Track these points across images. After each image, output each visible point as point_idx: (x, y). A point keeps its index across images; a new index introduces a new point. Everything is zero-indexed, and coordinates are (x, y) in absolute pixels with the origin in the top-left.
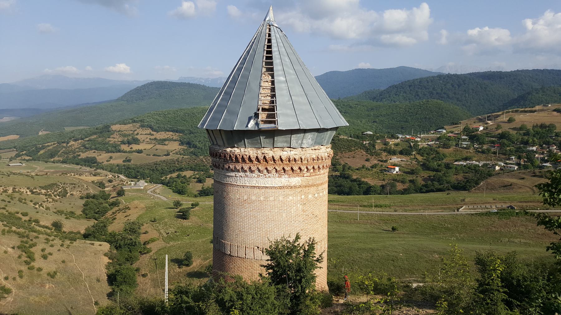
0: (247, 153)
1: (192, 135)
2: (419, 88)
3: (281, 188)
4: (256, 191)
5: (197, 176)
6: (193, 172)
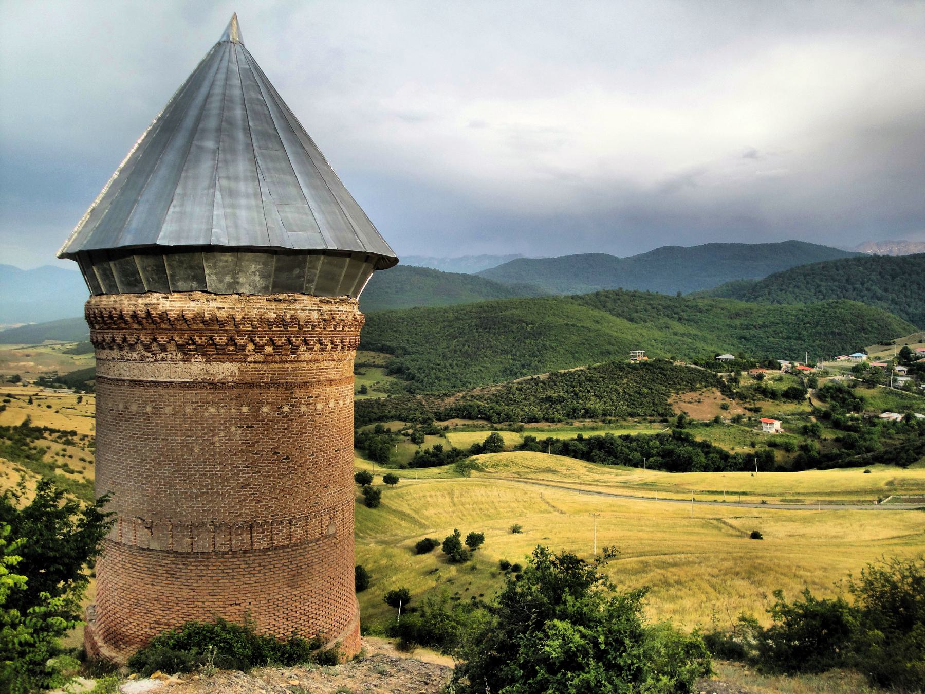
0: (117, 306)
1: (408, 357)
2: (821, 280)
3: (185, 386)
4: (138, 391)
5: (410, 431)
6: (404, 423)
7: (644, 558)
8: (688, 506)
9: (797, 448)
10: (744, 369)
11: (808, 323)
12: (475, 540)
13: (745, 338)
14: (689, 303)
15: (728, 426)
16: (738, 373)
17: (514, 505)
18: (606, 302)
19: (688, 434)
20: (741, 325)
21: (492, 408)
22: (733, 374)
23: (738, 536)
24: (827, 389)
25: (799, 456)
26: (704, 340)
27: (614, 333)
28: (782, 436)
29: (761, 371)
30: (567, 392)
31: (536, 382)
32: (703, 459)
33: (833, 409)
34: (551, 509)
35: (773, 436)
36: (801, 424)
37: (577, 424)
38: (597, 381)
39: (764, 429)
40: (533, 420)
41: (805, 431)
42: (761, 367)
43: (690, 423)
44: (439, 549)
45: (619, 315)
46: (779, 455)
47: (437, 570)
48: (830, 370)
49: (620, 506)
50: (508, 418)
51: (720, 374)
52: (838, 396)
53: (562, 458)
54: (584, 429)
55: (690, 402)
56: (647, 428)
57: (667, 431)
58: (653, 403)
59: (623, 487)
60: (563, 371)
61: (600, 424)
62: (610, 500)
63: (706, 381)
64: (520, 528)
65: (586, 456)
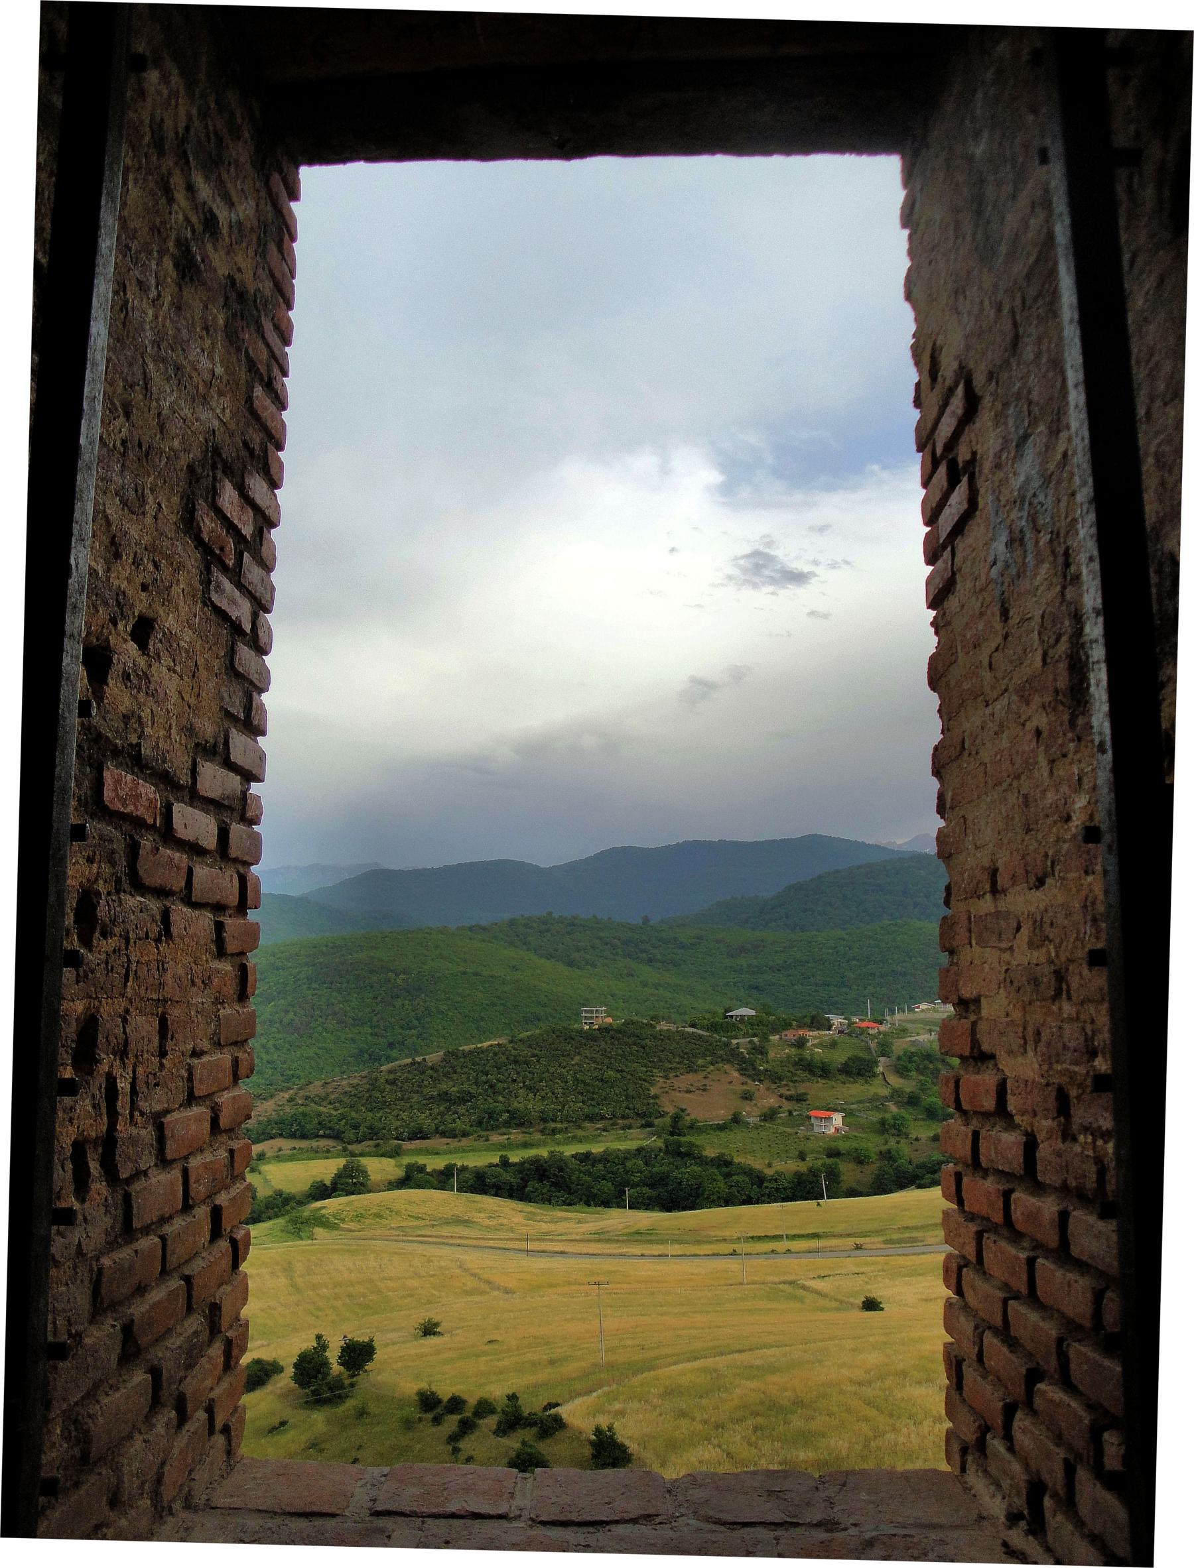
7: (709, 1362)
8: (732, 1264)
9: (874, 1157)
10: (774, 1031)
11: (854, 959)
12: (358, 1355)
15: (757, 1127)
16: (765, 1039)
17: (414, 1283)
19: (691, 1144)
20: (749, 966)
21: (343, 1116)
22: (756, 1039)
23: (837, 1309)
24: (910, 1057)
25: (881, 1168)
28: (846, 1138)
29: (801, 1033)
30: (476, 1083)
31: (421, 1067)
33: (923, 1088)
34: (483, 1286)
35: (832, 1138)
36: (875, 1117)
37: (496, 1138)
39: (816, 1129)
40: (418, 1134)
41: (883, 1127)
42: (799, 1027)
43: (691, 1127)
44: (285, 1380)
45: (549, 957)
46: (848, 1172)
47: (283, 1424)
48: (908, 1026)
49: (610, 1272)
50: (373, 1133)
51: (734, 1041)
52: (926, 1068)
53: (478, 1197)
54: (509, 1146)
56: (619, 1139)
57: (654, 1142)
58: (627, 1097)
59: (599, 1241)
60: (466, 1048)
61: (538, 1136)
62: (585, 1263)
64: (437, 1325)
65: (516, 1192)
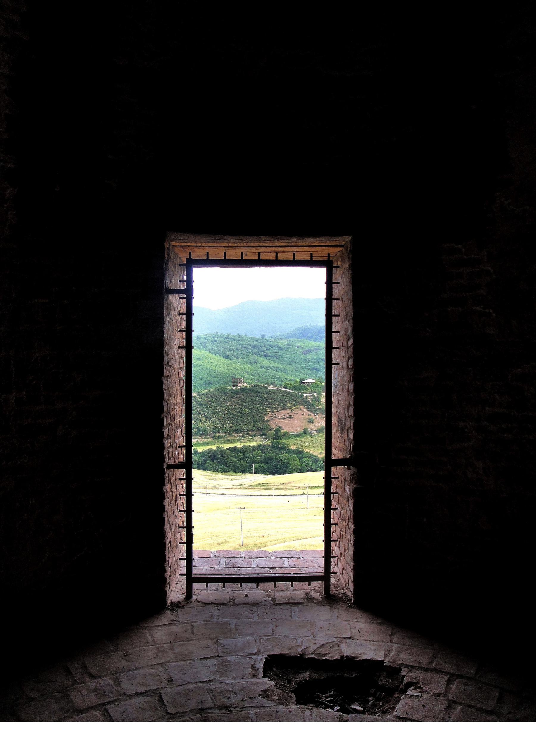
13: (316, 369)
14: (271, 343)
18: (205, 343)
19: (284, 443)
22: (315, 394)
26: (285, 371)
27: (214, 368)
32: (298, 463)
38: (206, 405)
51: (305, 395)
55: (283, 419)
56: (250, 441)
61: (211, 440)
63: (294, 401)
